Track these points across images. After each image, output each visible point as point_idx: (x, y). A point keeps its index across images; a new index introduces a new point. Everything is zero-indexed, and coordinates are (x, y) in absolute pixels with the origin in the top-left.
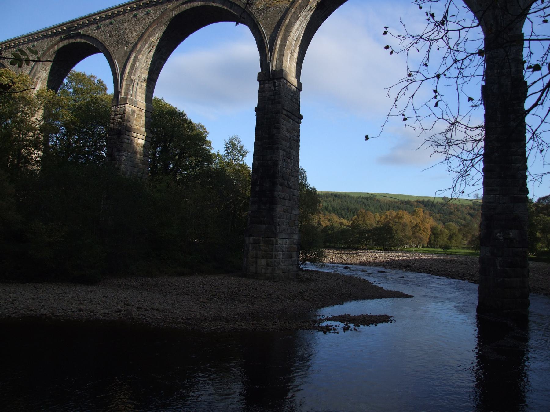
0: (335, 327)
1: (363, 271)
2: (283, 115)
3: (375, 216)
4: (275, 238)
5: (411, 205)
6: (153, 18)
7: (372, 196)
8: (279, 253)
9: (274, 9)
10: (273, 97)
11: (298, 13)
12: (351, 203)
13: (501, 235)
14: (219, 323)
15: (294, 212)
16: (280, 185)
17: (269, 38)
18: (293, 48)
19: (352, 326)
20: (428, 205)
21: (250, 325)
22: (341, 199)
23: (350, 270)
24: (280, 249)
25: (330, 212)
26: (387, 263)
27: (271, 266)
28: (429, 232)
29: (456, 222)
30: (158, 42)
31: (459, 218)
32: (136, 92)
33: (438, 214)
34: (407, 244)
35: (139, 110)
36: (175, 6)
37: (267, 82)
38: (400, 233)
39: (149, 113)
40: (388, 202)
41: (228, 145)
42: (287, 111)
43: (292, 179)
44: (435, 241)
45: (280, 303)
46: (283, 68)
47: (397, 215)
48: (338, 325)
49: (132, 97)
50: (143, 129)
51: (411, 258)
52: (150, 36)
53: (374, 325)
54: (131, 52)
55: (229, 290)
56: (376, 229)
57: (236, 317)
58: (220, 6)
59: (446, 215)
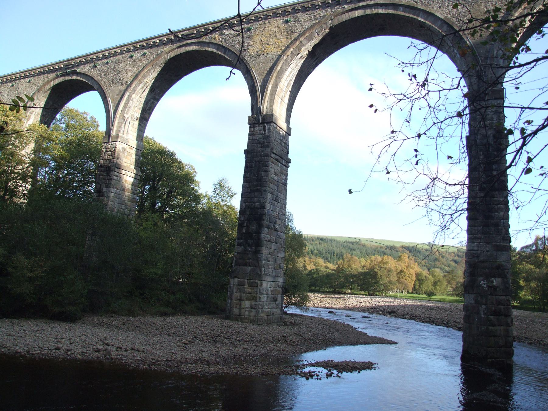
0: (317, 373)
1: (347, 316)
2: (271, 158)
3: (360, 261)
4: (260, 280)
5: (397, 251)
6: (149, 60)
7: (358, 241)
9: (266, 56)
10: (262, 140)
11: (289, 61)
12: (337, 247)
13: (485, 283)
14: (200, 366)
15: (279, 255)
17: (260, 83)
18: (283, 93)
19: (335, 372)
22: (327, 242)
23: (335, 314)
24: (264, 292)
25: (315, 256)
26: (372, 308)
27: (255, 309)
28: (414, 278)
29: (441, 269)
32: (128, 130)
35: (130, 148)
39: (140, 152)
40: (374, 247)
41: (216, 186)
42: (276, 154)
43: (279, 222)
44: (420, 287)
45: (263, 346)
46: (273, 112)
47: (382, 261)
49: (123, 134)
50: (133, 167)
51: (395, 304)
52: (144, 77)
53: (357, 372)
54: (126, 90)
55: (212, 332)
56: (361, 274)
57: (218, 360)
58: (215, 51)
59: (431, 262)
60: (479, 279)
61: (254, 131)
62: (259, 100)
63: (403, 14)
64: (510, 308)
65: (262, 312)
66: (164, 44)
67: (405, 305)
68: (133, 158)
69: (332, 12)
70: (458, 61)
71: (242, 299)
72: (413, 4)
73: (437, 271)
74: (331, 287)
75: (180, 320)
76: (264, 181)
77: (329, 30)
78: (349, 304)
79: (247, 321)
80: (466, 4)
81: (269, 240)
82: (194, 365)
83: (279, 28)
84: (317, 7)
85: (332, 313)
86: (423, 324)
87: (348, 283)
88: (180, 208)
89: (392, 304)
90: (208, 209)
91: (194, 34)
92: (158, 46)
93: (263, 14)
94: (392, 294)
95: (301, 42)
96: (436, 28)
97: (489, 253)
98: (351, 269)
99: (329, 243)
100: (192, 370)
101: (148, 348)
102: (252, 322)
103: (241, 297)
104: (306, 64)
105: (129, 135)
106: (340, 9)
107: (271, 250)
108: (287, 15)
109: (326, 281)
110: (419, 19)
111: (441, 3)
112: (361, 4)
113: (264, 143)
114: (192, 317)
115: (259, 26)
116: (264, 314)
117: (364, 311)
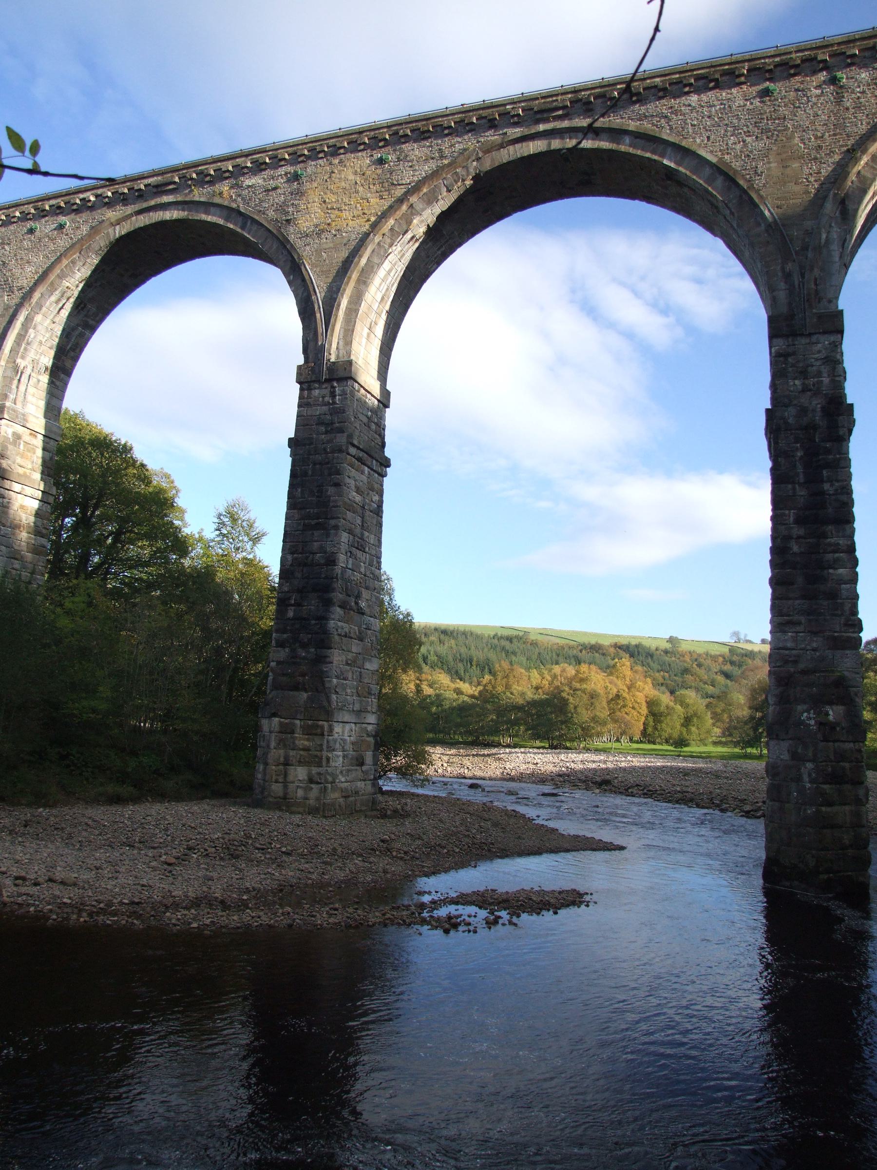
0: (467, 918)
1: (510, 793)
2: (349, 457)
3: (529, 676)
4: (328, 721)
5: (603, 654)
6: (71, 238)
7: (521, 634)
8: (335, 755)
9: (335, 235)
10: (328, 417)
11: (387, 246)
12: (476, 647)
13: (812, 715)
14: (208, 913)
15: (368, 666)
16: (340, 606)
17: (323, 294)
18: (373, 316)
19: (504, 914)
20: (638, 655)
21: (279, 917)
22: (455, 638)
23: (483, 790)
24: (337, 746)
25: (432, 667)
26: (560, 775)
27: (318, 783)
28: (644, 711)
29: (697, 690)
30: (80, 289)
31: (701, 680)
32: (25, 394)
33: (658, 671)
34: (599, 735)
35: (31, 434)
36: (120, 217)
37: (317, 385)
38: (584, 712)
39: (52, 442)
40: (555, 647)
41: (222, 517)
42: (358, 448)
43: (365, 594)
44: (655, 728)
45: (339, 864)
46: (352, 357)
47: (576, 675)
48: (473, 914)
49: (15, 404)
50: (37, 476)
51: (610, 765)
52: (61, 277)
53: (551, 912)
54: (19, 306)
55: (226, 836)
56: (533, 703)
57: (245, 897)
58: (221, 222)
59: (675, 675)
60: (800, 708)
61: (309, 397)
62: (320, 331)
63: (631, 150)
64: (863, 766)
65: (334, 789)
66: (106, 204)
67: (630, 767)
68: (37, 457)
69: (478, 142)
70: (747, 254)
71: (290, 762)
72: (651, 130)
73: (691, 695)
74: (469, 733)
75: (154, 810)
76: (335, 507)
77: (472, 182)
78: (511, 767)
79: (301, 809)
80: (762, 133)
81: (346, 633)
82: (193, 911)
83: (363, 174)
84: (446, 132)
85: (477, 788)
86: (670, 805)
87: (506, 723)
88: (143, 567)
89: (603, 766)
90: (205, 568)
91: (175, 183)
92: (92, 208)
93: (327, 144)
94: (600, 745)
95: (412, 205)
96: (701, 182)
97: (818, 654)
98: (512, 693)
99: (461, 639)
100: (190, 923)
101: (86, 876)
102: (313, 811)
103: (286, 758)
104: (423, 254)
105: (29, 405)
106: (496, 137)
107: (350, 656)
108: (381, 147)
109: (459, 720)
110: (666, 162)
111: (710, 130)
112: (542, 127)
113: (332, 423)
114: (179, 805)
115: (319, 170)
116: (336, 795)
117: (544, 782)
